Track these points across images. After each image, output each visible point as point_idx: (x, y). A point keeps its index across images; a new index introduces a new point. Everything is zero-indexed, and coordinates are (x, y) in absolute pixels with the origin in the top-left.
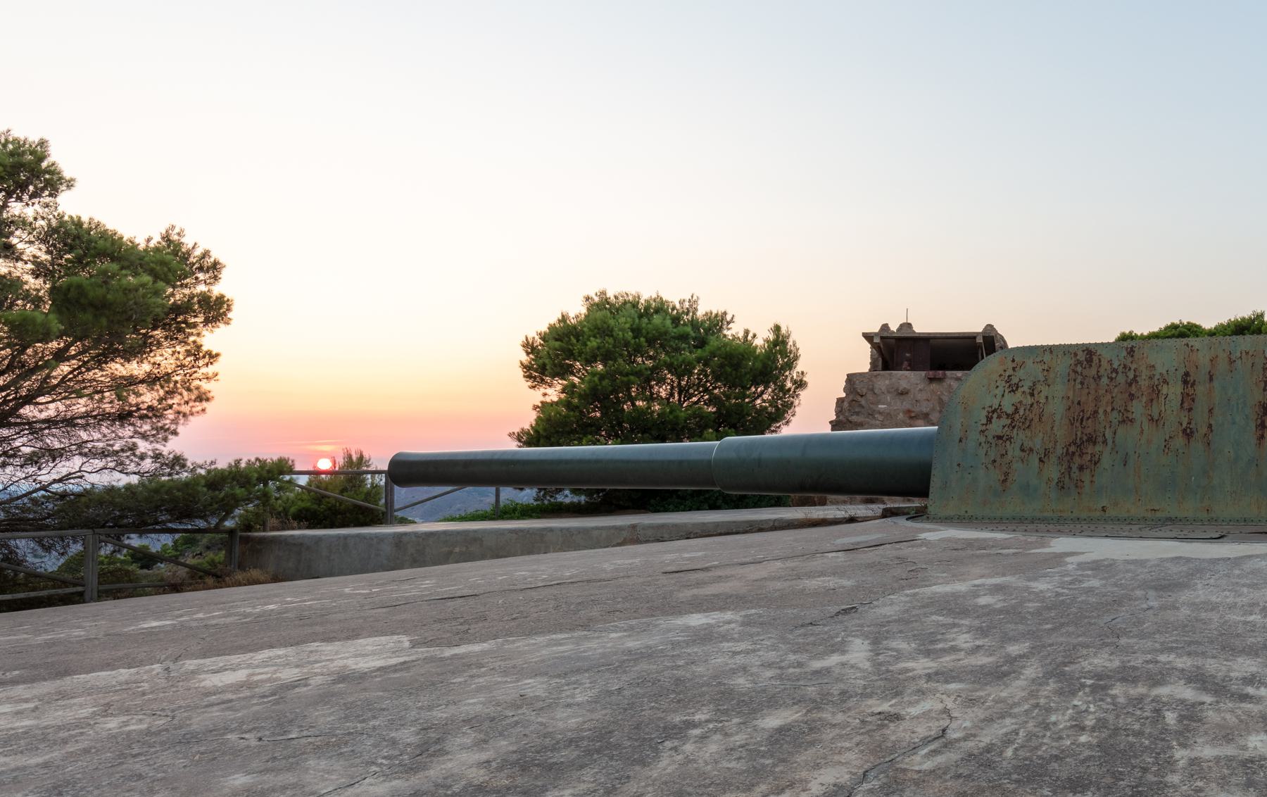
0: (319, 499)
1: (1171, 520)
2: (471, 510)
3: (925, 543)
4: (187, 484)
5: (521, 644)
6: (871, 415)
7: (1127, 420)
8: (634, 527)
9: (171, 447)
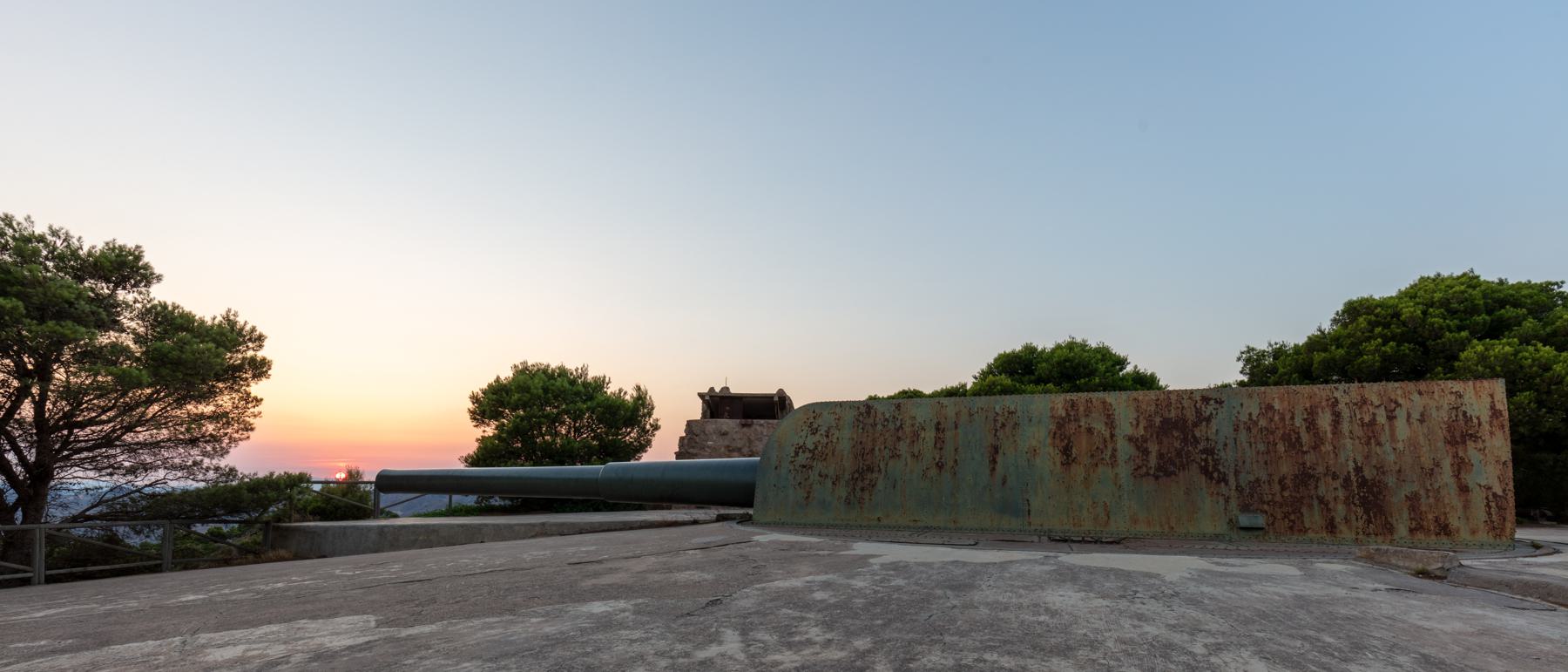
0: (328, 500)
1: (928, 529)
2: (431, 509)
3: (758, 544)
4: (234, 489)
5: (462, 626)
6: (703, 448)
7: (895, 456)
8: (543, 524)
9: (223, 463)
